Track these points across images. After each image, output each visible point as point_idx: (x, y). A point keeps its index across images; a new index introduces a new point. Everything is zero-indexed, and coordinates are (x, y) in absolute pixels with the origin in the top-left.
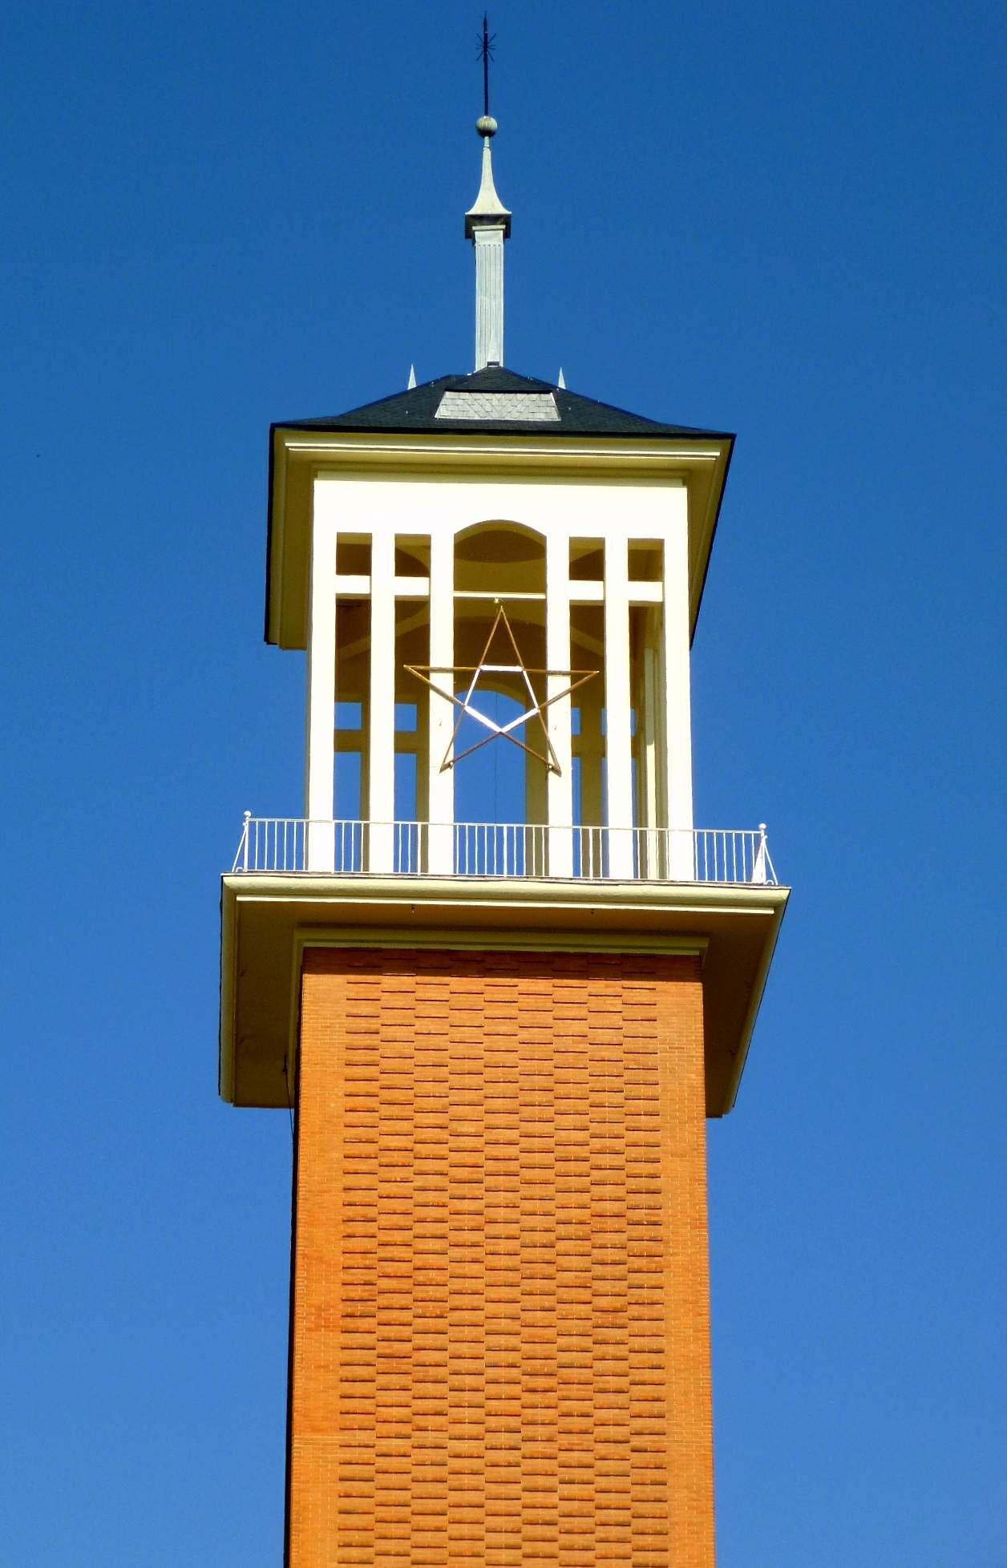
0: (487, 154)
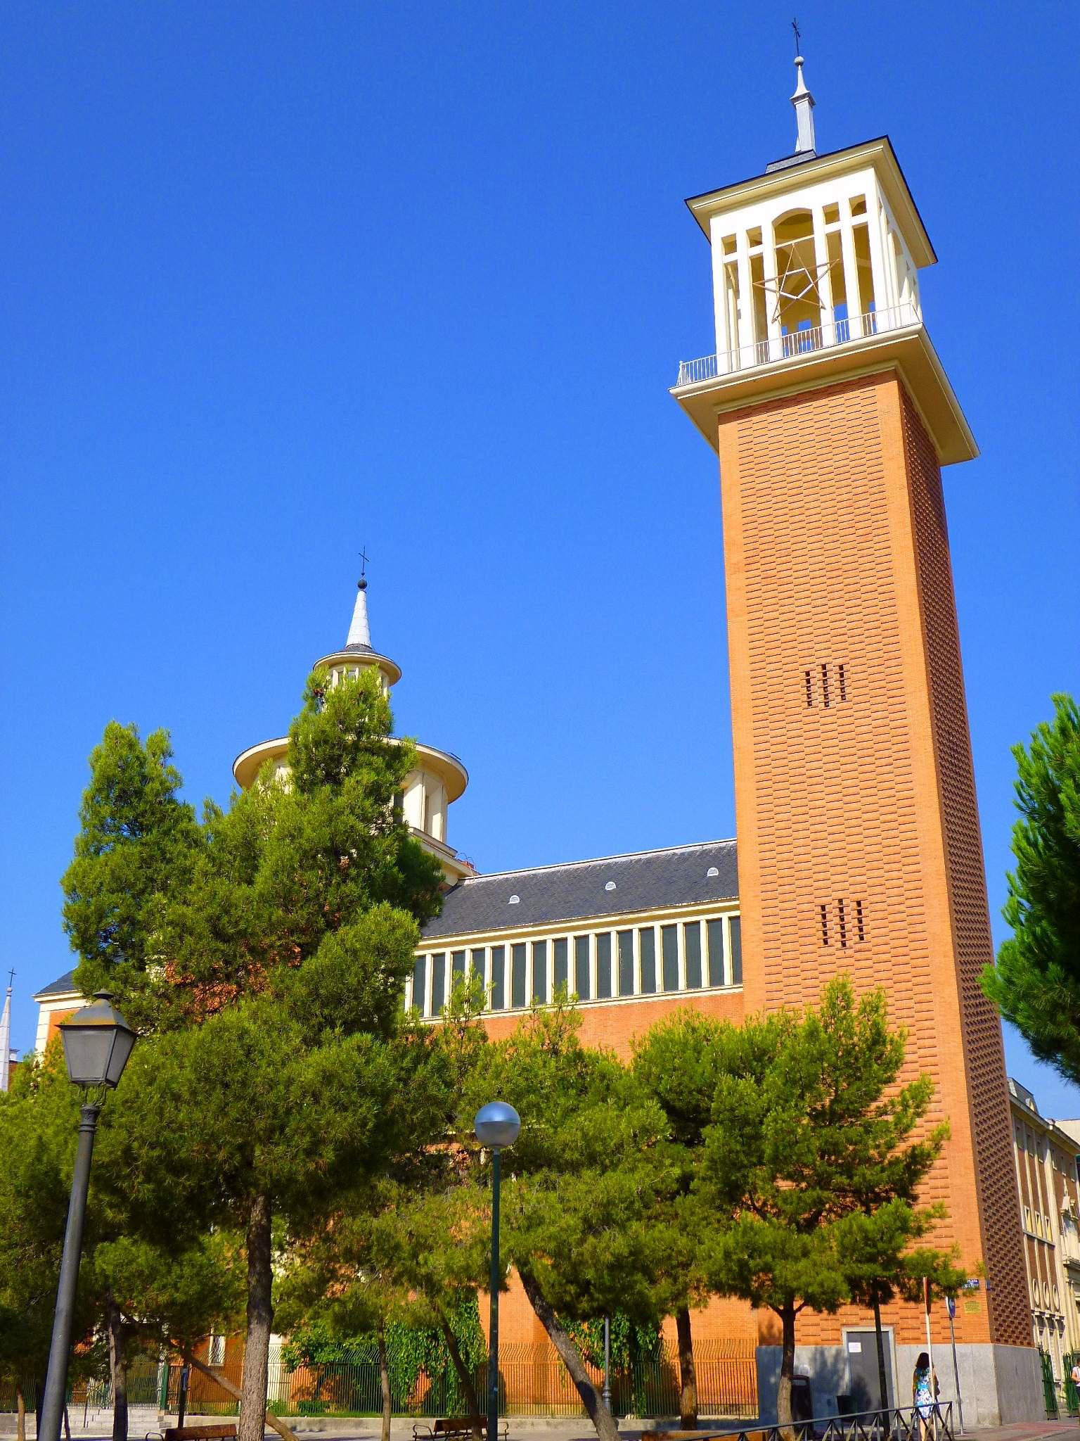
0: (800, 72)
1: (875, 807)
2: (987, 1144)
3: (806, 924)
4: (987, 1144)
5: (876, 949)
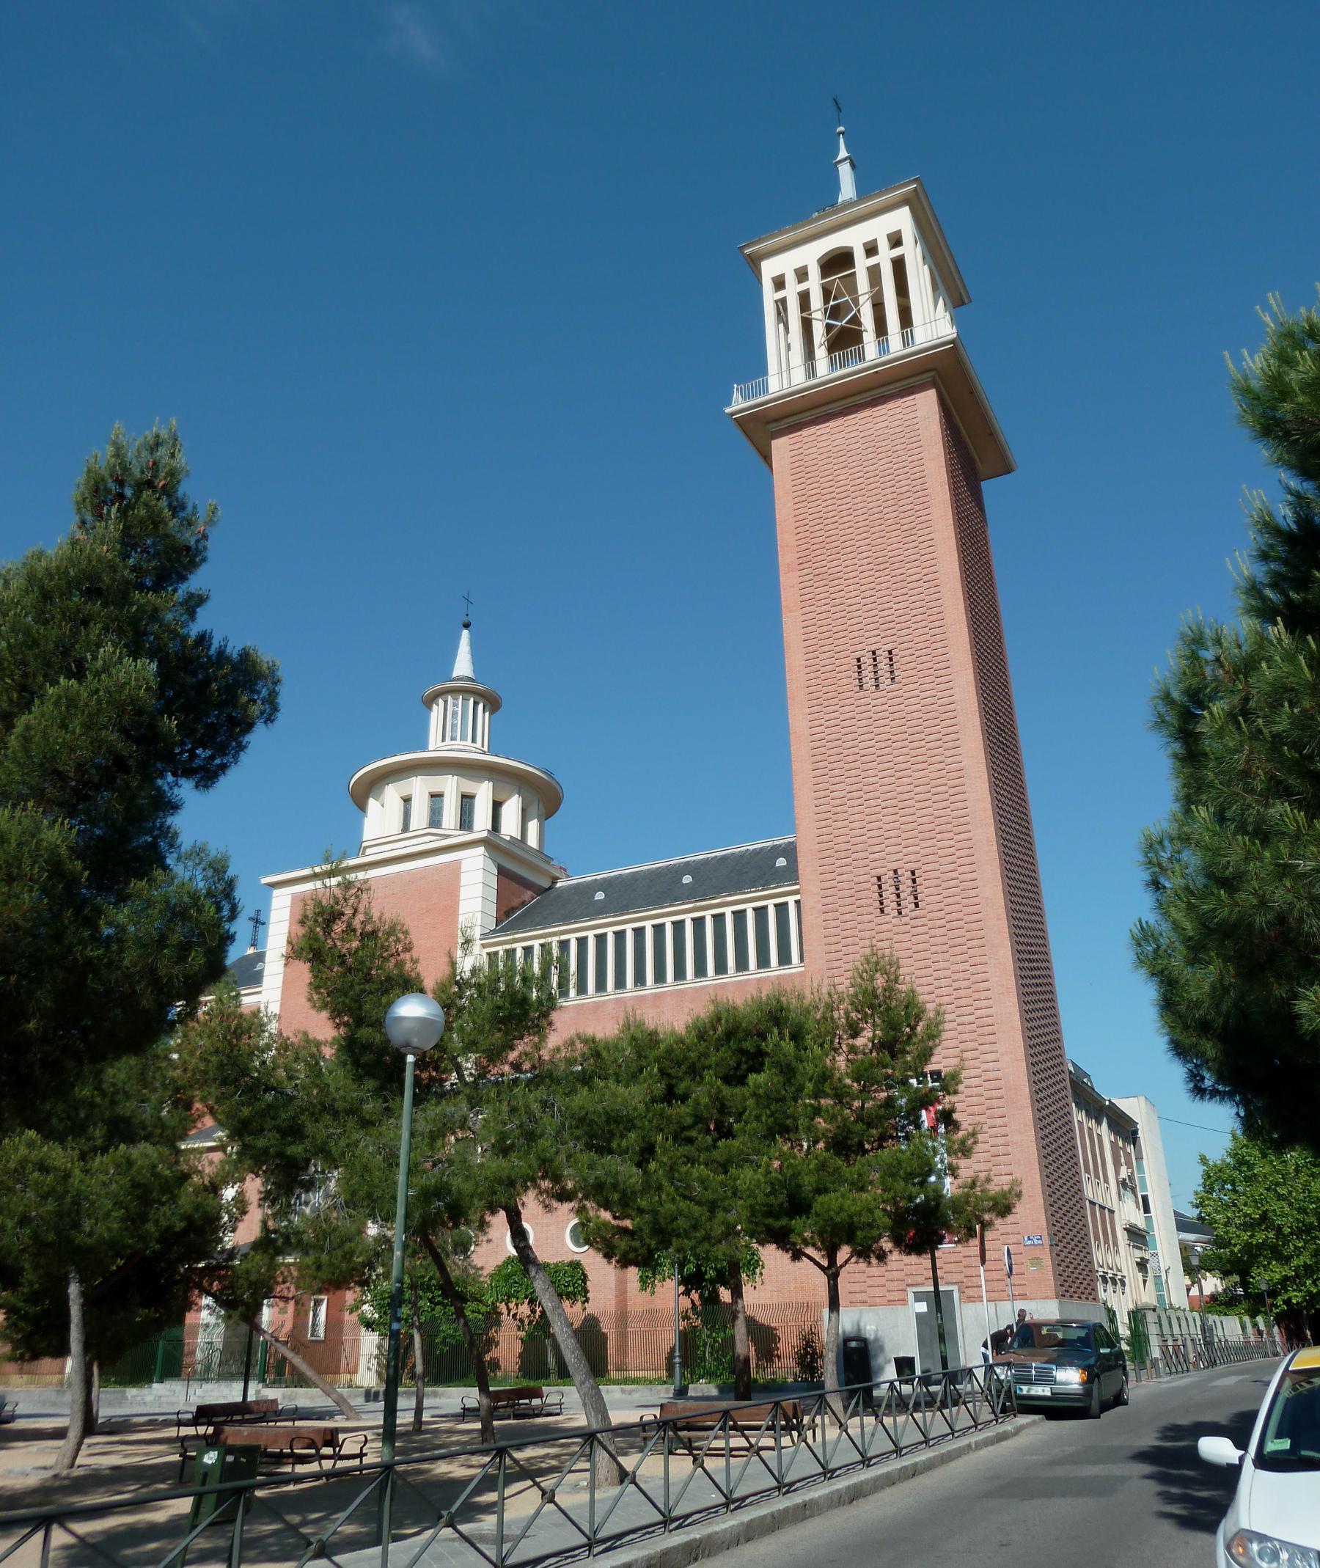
0: (842, 140)
1: (926, 780)
2: (1046, 1102)
3: (863, 894)
4: (1046, 1102)
5: (931, 916)
